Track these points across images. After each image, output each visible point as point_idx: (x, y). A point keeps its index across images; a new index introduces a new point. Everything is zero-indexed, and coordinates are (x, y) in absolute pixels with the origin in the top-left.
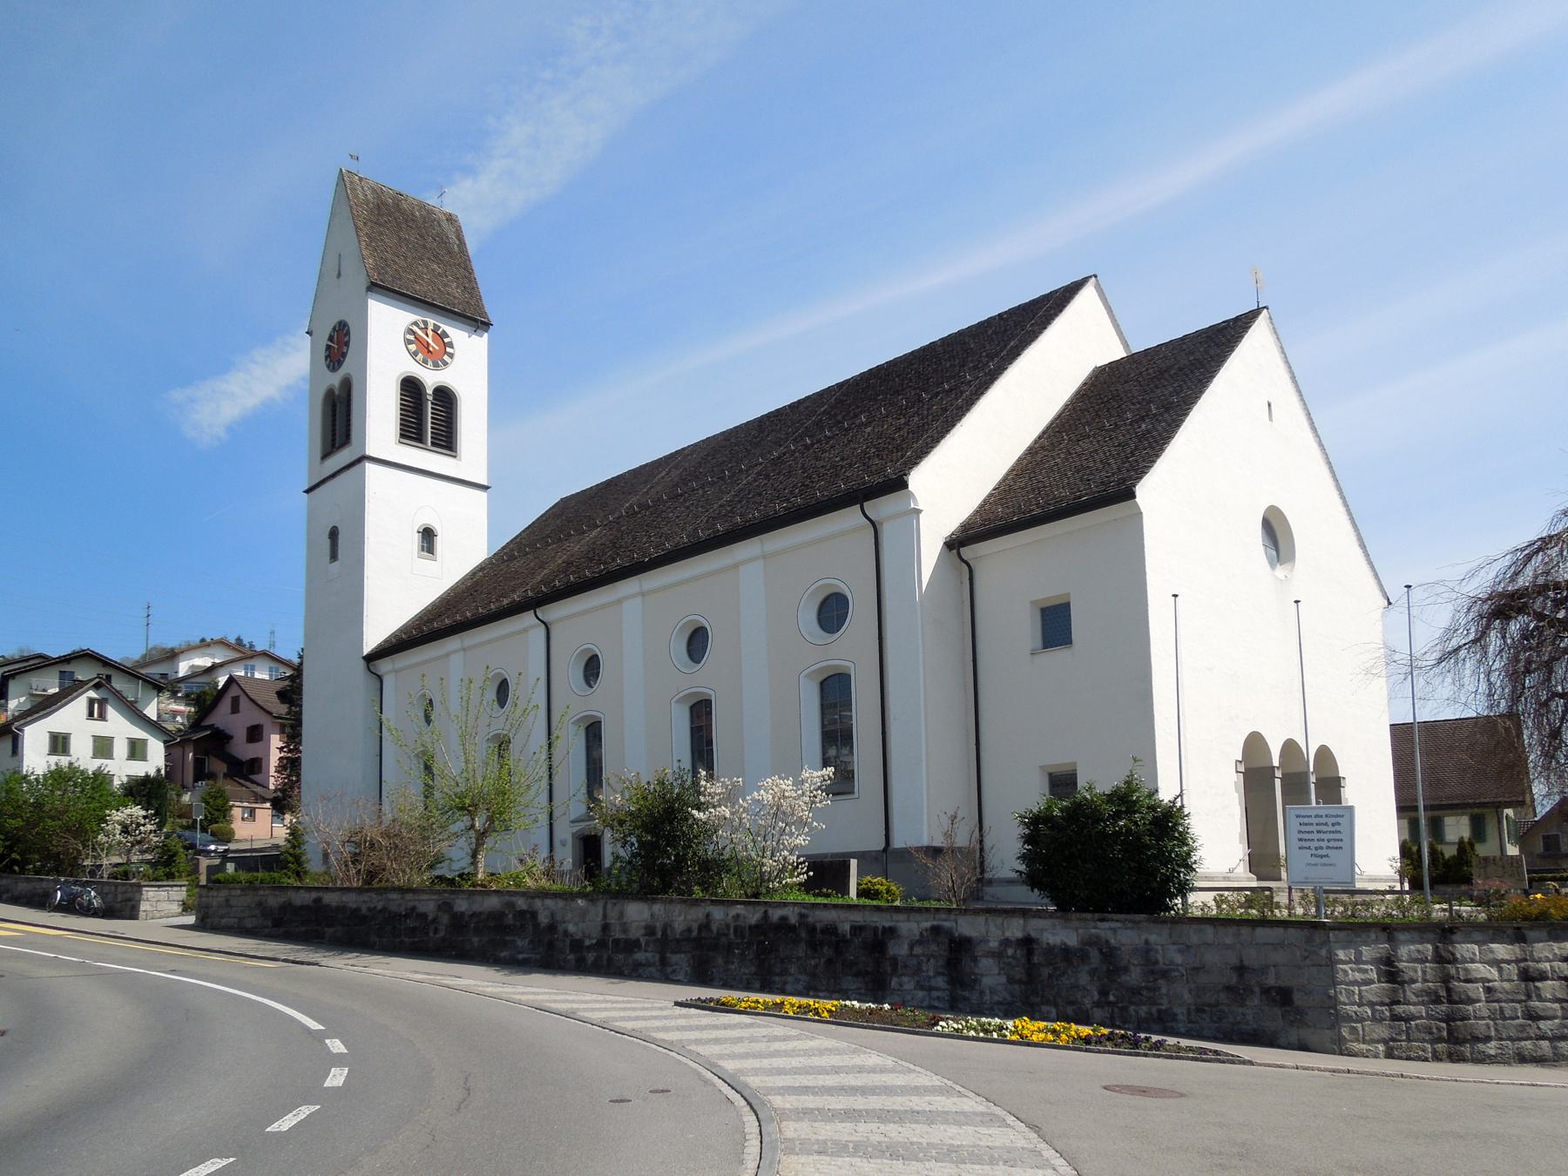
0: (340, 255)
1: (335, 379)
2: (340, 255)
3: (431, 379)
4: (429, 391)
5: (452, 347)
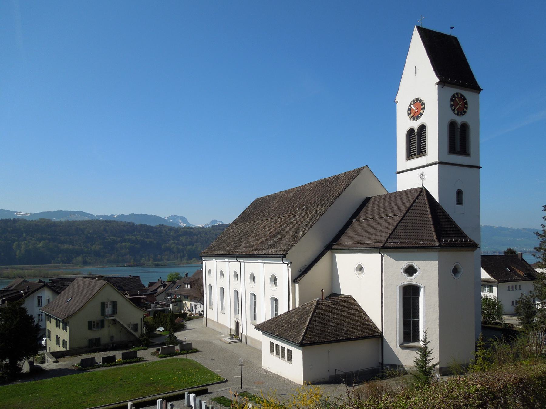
0: (416, 67)
1: (416, 125)
2: (416, 67)
3: (460, 120)
4: (459, 127)
5: (467, 104)
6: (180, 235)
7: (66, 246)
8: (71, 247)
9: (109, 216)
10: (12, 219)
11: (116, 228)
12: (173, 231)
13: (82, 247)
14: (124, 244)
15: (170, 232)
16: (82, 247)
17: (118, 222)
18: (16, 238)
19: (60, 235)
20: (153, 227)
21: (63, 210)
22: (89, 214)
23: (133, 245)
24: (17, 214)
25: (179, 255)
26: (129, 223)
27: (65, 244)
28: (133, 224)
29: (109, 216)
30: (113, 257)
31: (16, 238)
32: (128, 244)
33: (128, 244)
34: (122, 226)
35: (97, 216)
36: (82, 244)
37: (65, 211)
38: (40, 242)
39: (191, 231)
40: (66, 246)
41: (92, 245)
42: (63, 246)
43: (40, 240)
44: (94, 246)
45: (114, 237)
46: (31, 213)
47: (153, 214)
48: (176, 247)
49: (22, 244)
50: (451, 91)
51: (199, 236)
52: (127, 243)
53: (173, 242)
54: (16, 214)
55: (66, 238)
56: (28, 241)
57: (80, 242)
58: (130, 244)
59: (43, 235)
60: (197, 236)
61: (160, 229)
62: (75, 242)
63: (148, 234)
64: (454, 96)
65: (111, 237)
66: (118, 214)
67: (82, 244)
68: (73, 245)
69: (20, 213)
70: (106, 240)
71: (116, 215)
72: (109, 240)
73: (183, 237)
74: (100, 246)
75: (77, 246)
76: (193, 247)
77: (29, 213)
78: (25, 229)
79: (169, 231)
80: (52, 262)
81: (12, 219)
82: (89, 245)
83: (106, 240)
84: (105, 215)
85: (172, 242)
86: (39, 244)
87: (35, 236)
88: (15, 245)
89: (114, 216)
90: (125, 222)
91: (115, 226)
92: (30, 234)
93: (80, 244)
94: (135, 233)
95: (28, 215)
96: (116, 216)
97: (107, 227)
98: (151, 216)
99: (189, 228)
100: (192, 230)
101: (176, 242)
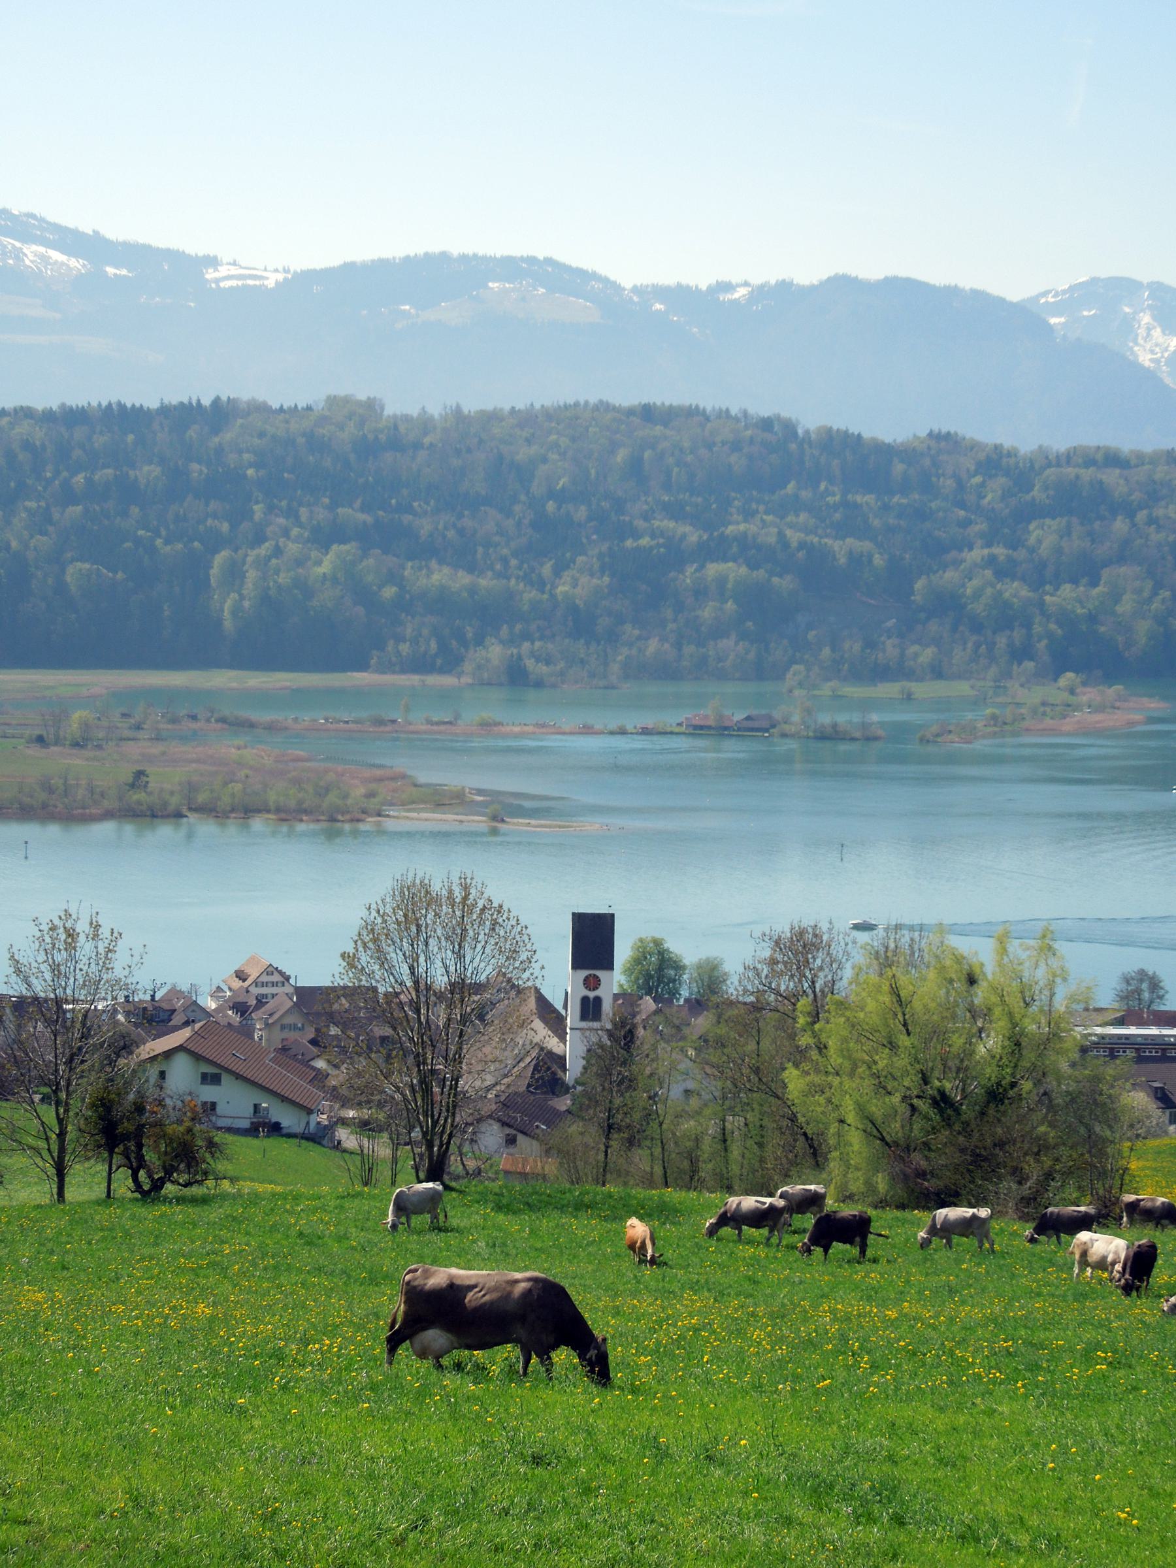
3: (592, 995)
6: (1035, 512)
7: (439, 576)
8: (464, 579)
9: (704, 287)
10: (206, 402)
11: (690, 458)
12: (1002, 480)
13: (513, 581)
14: (713, 569)
15: (983, 485)
16: (513, 581)
17: (708, 419)
18: (225, 527)
19: (415, 504)
20: (885, 452)
21: (455, 250)
22: (595, 276)
23: (761, 574)
24: (217, 275)
25: (1002, 641)
26: (767, 424)
27: (434, 564)
28: (789, 427)
29: (704, 287)
30: (653, 646)
31: (225, 527)
32: (733, 571)
33: (733, 571)
34: (724, 443)
35: (635, 290)
36: (514, 562)
37: (464, 258)
38: (326, 548)
39: (1101, 482)
40: (439, 576)
41: (558, 572)
42: (424, 572)
43: (324, 538)
44: (567, 575)
45: (672, 524)
46: (286, 271)
47: (967, 282)
48: (989, 591)
49: (249, 559)
50: (583, 974)
51: (1142, 516)
52: (730, 564)
53: (986, 551)
54: (210, 275)
55: (441, 526)
56: (273, 543)
57: (505, 551)
58: (743, 570)
59: (340, 510)
60: (1131, 514)
61: (927, 462)
62: (480, 550)
63: (859, 499)
64: (587, 977)
65: (656, 523)
66: (757, 280)
67: (514, 562)
68: (471, 569)
69: (234, 271)
70: (629, 543)
71: (746, 284)
72: (645, 541)
73: (1048, 521)
74: (595, 581)
75: (490, 574)
76: (1096, 591)
77: (276, 271)
78: (262, 473)
79: (978, 479)
80: (373, 662)
81: (206, 402)
82: (547, 570)
83: (629, 543)
84: (679, 286)
85: (977, 554)
86: (319, 563)
87: (304, 512)
88: (220, 559)
89: (728, 287)
90: (745, 413)
91: (686, 444)
92: (284, 503)
93: (505, 561)
94: (791, 487)
95: (270, 283)
96: (741, 292)
97: (647, 454)
98: (952, 291)
99: (1099, 457)
100: (1111, 477)
101: (1000, 551)
